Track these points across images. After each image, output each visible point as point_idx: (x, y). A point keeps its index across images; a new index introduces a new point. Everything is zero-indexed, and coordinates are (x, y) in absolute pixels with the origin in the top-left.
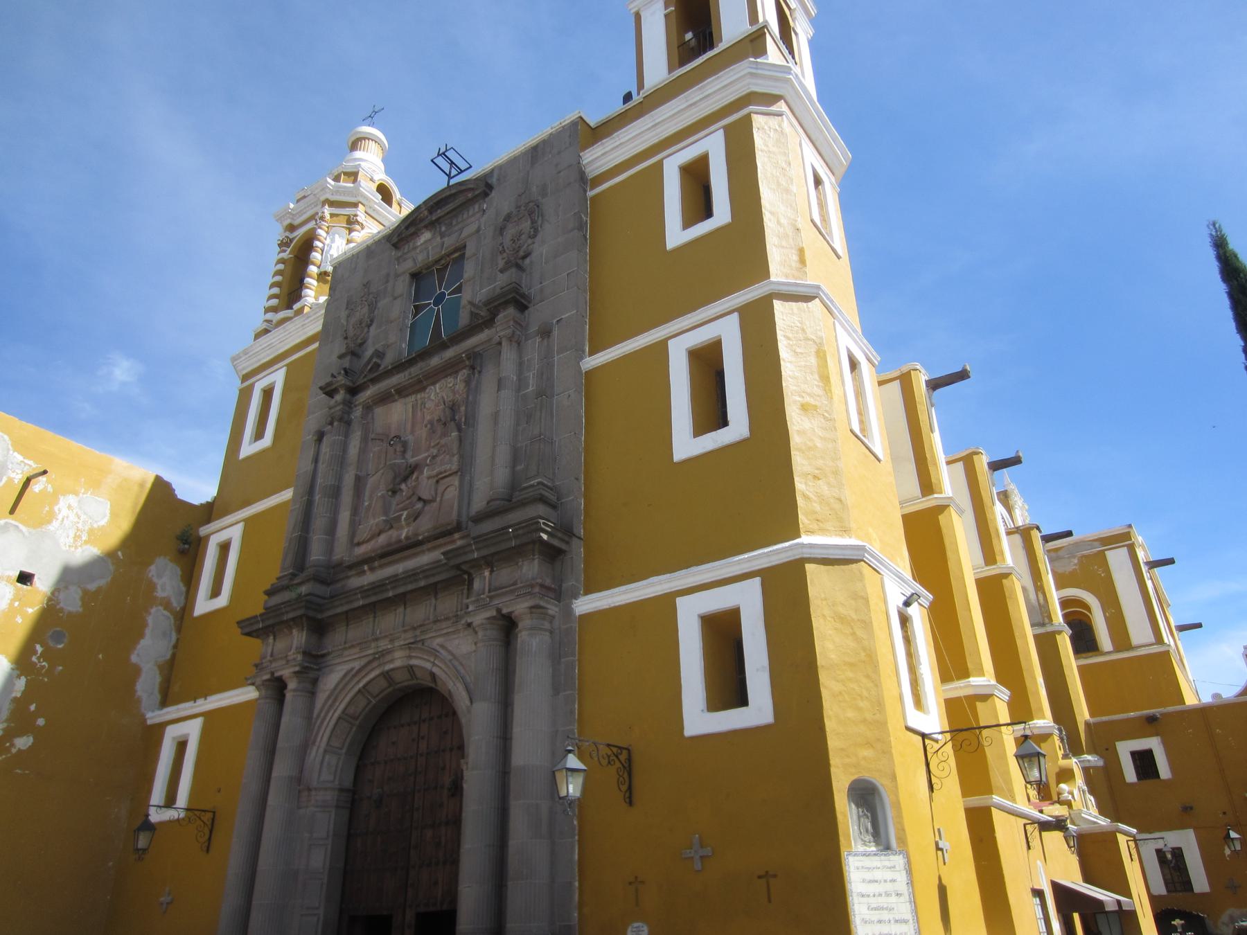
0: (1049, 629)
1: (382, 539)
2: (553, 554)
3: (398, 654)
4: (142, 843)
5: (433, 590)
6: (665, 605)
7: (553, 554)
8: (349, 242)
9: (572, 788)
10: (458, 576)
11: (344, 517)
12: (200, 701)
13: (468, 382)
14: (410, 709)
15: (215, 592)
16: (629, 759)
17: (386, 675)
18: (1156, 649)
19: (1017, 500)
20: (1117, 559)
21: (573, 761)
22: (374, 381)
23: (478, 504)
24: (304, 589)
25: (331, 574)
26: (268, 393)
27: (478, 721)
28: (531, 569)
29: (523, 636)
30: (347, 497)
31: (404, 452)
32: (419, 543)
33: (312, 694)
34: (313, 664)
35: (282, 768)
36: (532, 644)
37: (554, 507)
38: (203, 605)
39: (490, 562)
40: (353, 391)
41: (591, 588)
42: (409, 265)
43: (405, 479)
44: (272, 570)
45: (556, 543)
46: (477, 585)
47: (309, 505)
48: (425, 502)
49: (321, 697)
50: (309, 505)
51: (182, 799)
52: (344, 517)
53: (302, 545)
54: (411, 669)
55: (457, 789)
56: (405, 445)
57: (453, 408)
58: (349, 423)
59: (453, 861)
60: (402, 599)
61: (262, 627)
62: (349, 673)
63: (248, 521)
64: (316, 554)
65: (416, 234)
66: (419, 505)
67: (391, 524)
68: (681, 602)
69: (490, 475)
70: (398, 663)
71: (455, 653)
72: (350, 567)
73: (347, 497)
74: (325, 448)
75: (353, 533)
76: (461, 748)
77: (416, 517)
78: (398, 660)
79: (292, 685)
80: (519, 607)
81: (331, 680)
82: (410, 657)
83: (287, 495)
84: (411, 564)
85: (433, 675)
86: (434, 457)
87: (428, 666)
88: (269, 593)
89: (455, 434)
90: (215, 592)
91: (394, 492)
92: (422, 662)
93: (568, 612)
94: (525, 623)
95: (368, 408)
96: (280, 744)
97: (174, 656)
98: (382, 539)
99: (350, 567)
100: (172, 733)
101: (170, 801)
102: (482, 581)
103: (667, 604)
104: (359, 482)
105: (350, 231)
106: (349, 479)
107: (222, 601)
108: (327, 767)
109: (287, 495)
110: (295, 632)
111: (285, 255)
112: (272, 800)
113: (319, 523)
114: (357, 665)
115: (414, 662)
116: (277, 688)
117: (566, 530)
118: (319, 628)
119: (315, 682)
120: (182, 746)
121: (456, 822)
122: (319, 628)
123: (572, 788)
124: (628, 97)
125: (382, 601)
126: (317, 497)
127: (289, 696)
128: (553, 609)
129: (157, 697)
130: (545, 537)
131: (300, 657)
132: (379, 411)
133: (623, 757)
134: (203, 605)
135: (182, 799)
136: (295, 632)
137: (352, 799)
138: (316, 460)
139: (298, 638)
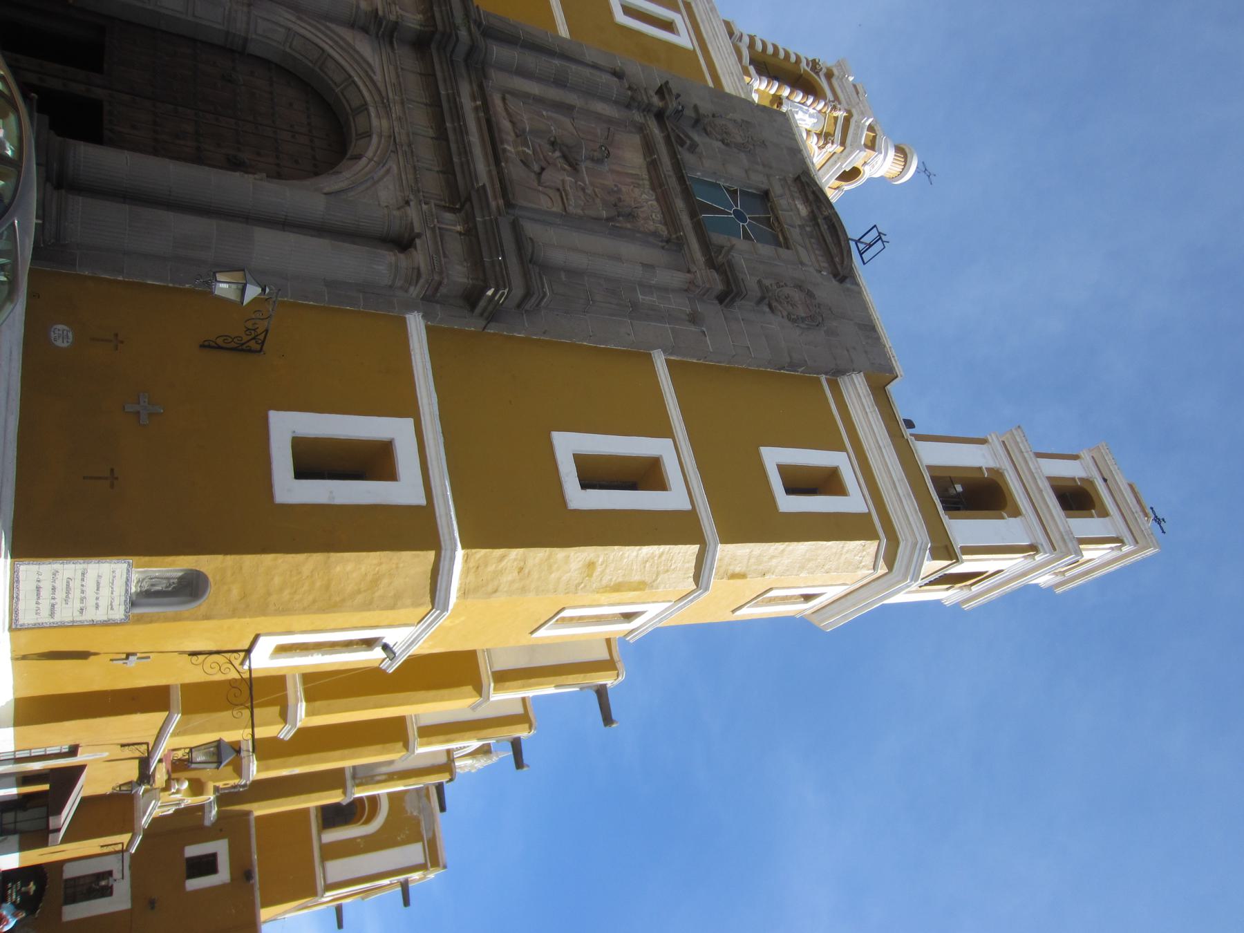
0: (349, 783)
2: (471, 299)
3: (385, 123)
5: (448, 170)
7: (471, 299)
8: (808, 132)
11: (534, 88)
13: (655, 234)
16: (250, 351)
17: (364, 107)
18: (320, 883)
19: (481, 763)
20: (414, 853)
21: (253, 292)
22: (668, 139)
23: (531, 229)
24: (463, 33)
25: (477, 66)
26: (669, 26)
28: (459, 274)
30: (554, 93)
31: (592, 160)
36: (381, 266)
37: (519, 306)
39: (470, 232)
40: (660, 116)
42: (777, 189)
43: (564, 157)
45: (482, 303)
46: (448, 216)
48: (539, 174)
49: (342, 31)
52: (534, 88)
53: (510, 38)
54: (368, 135)
55: (235, 164)
56: (599, 161)
59: (156, 149)
60: (441, 135)
64: (498, 52)
65: (806, 201)
66: (536, 168)
67: (520, 135)
68: (409, 423)
69: (560, 245)
70: (375, 122)
71: (379, 184)
72: (481, 87)
73: (554, 93)
76: (278, 175)
77: (525, 163)
78: (379, 123)
80: (420, 257)
81: (365, 47)
82: (380, 136)
83: (563, 31)
84: (477, 151)
87: (370, 153)
89: (604, 214)
92: (373, 147)
93: (411, 307)
94: (403, 260)
95: (641, 129)
98: (506, 124)
102: (453, 223)
104: (567, 109)
105: (819, 135)
106: (572, 98)
109: (563, 31)
111: (804, 64)
113: (531, 61)
114: (378, 78)
115: (375, 139)
117: (494, 315)
119: (365, 30)
121: (199, 159)
122: (421, 43)
123: (224, 287)
124: (909, 424)
125: (442, 113)
130: (490, 293)
131: (393, 18)
132: (637, 139)
133: (253, 345)
136: (420, 17)
137: (234, 50)
138: (595, 67)
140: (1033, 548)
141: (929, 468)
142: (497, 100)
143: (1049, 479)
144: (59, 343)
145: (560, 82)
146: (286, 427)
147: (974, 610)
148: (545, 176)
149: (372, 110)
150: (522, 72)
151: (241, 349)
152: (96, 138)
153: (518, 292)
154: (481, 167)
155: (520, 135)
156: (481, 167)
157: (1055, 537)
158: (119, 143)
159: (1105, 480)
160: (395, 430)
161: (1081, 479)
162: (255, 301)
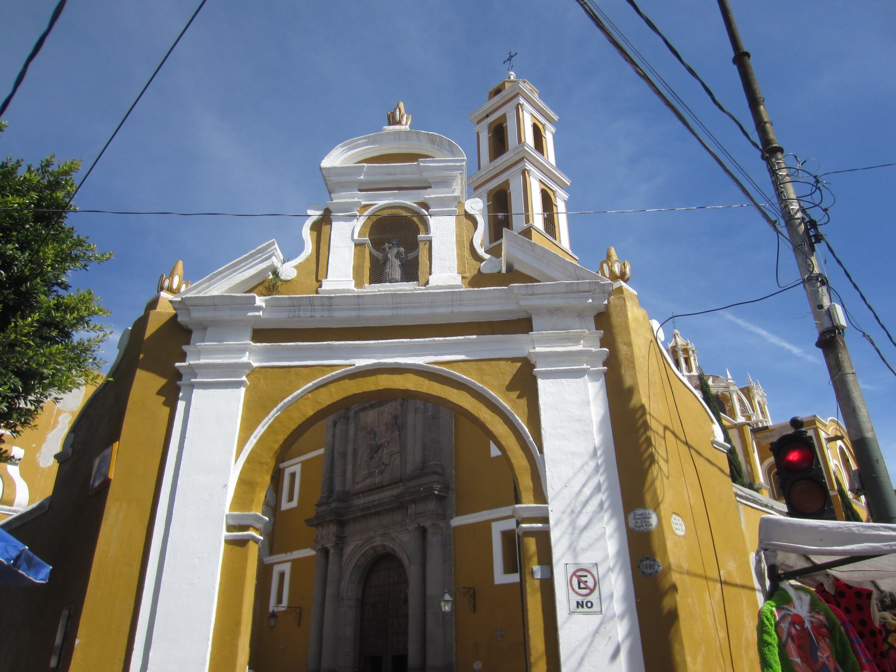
1: (367, 482)
2: (441, 499)
3: (378, 539)
4: (272, 622)
5: (391, 510)
6: (486, 526)
7: (441, 499)
9: (447, 608)
10: (400, 505)
11: (349, 468)
12: (289, 554)
13: (402, 405)
14: (382, 562)
15: (291, 499)
16: (474, 593)
17: (373, 548)
19: (759, 395)
21: (447, 597)
23: (409, 469)
24: (333, 505)
25: (346, 497)
27: (413, 572)
28: (431, 506)
29: (429, 537)
30: (350, 458)
31: (375, 438)
32: (385, 486)
33: (341, 555)
34: (341, 541)
35: (330, 590)
36: (433, 539)
37: (442, 475)
38: (285, 506)
39: (414, 501)
41: (459, 514)
43: (376, 452)
44: (317, 494)
45: (442, 494)
46: (409, 511)
47: (332, 453)
48: (386, 465)
49: (345, 558)
50: (332, 453)
51: (285, 602)
52: (349, 468)
53: (331, 481)
54: (384, 546)
55: (406, 601)
56: (375, 434)
57: (396, 418)
58: (348, 419)
59: (406, 633)
60: (378, 513)
61: (317, 522)
62: (359, 544)
63: (304, 463)
64: (338, 487)
66: (383, 467)
67: (371, 475)
68: (494, 525)
69: (413, 458)
70: (378, 543)
71: (403, 542)
72: (354, 495)
73: (350, 458)
74: (338, 431)
75: (354, 479)
76: (406, 582)
77: (382, 472)
78: (378, 541)
79: (332, 551)
80: (427, 524)
81: (349, 549)
82: (693, 352)
83: (321, 451)
84: (382, 495)
85: (393, 550)
86: (389, 443)
87: (391, 545)
88: (318, 505)
89: (397, 432)
90: (291, 499)
91: (372, 458)
92: (388, 543)
93: (448, 525)
94: (430, 531)
95: (357, 413)
96: (329, 579)
97: (273, 529)
98: (367, 482)
99: (354, 495)
100: (277, 569)
101: (279, 600)
102: (412, 509)
103: (486, 526)
104: (355, 451)
106: (350, 449)
107: (294, 504)
108: (350, 590)
109: (321, 451)
110: (331, 526)
112: (327, 604)
113: (338, 471)
114: (360, 542)
115: (385, 543)
116: (325, 552)
117: (446, 487)
118: (342, 524)
119: (342, 549)
120: (282, 575)
121: (406, 616)
122: (342, 524)
123: (447, 608)
125: (370, 512)
126: (336, 456)
127: (331, 556)
128: (442, 524)
129: (268, 550)
130: (436, 492)
131: (334, 538)
132: (362, 414)
133: (471, 592)
134: (285, 506)
135: (285, 602)
136: (331, 526)
137: (362, 603)
138: (334, 437)
139: (333, 529)
140: (524, 172)
141: (490, 243)
142: (358, 487)
143: (491, 161)
144: (475, 666)
145: (344, 455)
146: (501, 577)
147: (568, 175)
148: (386, 461)
149: (374, 544)
150: (344, 473)
151: (474, 596)
152: (405, 657)
153: (435, 478)
154: (387, 494)
155: (371, 475)
156: (387, 494)
157: (517, 158)
158: (406, 648)
159: (487, 116)
160: (497, 529)
161: (489, 133)
162: (451, 596)
